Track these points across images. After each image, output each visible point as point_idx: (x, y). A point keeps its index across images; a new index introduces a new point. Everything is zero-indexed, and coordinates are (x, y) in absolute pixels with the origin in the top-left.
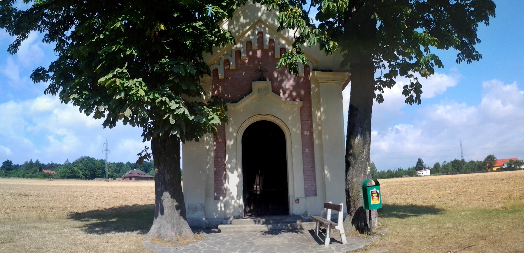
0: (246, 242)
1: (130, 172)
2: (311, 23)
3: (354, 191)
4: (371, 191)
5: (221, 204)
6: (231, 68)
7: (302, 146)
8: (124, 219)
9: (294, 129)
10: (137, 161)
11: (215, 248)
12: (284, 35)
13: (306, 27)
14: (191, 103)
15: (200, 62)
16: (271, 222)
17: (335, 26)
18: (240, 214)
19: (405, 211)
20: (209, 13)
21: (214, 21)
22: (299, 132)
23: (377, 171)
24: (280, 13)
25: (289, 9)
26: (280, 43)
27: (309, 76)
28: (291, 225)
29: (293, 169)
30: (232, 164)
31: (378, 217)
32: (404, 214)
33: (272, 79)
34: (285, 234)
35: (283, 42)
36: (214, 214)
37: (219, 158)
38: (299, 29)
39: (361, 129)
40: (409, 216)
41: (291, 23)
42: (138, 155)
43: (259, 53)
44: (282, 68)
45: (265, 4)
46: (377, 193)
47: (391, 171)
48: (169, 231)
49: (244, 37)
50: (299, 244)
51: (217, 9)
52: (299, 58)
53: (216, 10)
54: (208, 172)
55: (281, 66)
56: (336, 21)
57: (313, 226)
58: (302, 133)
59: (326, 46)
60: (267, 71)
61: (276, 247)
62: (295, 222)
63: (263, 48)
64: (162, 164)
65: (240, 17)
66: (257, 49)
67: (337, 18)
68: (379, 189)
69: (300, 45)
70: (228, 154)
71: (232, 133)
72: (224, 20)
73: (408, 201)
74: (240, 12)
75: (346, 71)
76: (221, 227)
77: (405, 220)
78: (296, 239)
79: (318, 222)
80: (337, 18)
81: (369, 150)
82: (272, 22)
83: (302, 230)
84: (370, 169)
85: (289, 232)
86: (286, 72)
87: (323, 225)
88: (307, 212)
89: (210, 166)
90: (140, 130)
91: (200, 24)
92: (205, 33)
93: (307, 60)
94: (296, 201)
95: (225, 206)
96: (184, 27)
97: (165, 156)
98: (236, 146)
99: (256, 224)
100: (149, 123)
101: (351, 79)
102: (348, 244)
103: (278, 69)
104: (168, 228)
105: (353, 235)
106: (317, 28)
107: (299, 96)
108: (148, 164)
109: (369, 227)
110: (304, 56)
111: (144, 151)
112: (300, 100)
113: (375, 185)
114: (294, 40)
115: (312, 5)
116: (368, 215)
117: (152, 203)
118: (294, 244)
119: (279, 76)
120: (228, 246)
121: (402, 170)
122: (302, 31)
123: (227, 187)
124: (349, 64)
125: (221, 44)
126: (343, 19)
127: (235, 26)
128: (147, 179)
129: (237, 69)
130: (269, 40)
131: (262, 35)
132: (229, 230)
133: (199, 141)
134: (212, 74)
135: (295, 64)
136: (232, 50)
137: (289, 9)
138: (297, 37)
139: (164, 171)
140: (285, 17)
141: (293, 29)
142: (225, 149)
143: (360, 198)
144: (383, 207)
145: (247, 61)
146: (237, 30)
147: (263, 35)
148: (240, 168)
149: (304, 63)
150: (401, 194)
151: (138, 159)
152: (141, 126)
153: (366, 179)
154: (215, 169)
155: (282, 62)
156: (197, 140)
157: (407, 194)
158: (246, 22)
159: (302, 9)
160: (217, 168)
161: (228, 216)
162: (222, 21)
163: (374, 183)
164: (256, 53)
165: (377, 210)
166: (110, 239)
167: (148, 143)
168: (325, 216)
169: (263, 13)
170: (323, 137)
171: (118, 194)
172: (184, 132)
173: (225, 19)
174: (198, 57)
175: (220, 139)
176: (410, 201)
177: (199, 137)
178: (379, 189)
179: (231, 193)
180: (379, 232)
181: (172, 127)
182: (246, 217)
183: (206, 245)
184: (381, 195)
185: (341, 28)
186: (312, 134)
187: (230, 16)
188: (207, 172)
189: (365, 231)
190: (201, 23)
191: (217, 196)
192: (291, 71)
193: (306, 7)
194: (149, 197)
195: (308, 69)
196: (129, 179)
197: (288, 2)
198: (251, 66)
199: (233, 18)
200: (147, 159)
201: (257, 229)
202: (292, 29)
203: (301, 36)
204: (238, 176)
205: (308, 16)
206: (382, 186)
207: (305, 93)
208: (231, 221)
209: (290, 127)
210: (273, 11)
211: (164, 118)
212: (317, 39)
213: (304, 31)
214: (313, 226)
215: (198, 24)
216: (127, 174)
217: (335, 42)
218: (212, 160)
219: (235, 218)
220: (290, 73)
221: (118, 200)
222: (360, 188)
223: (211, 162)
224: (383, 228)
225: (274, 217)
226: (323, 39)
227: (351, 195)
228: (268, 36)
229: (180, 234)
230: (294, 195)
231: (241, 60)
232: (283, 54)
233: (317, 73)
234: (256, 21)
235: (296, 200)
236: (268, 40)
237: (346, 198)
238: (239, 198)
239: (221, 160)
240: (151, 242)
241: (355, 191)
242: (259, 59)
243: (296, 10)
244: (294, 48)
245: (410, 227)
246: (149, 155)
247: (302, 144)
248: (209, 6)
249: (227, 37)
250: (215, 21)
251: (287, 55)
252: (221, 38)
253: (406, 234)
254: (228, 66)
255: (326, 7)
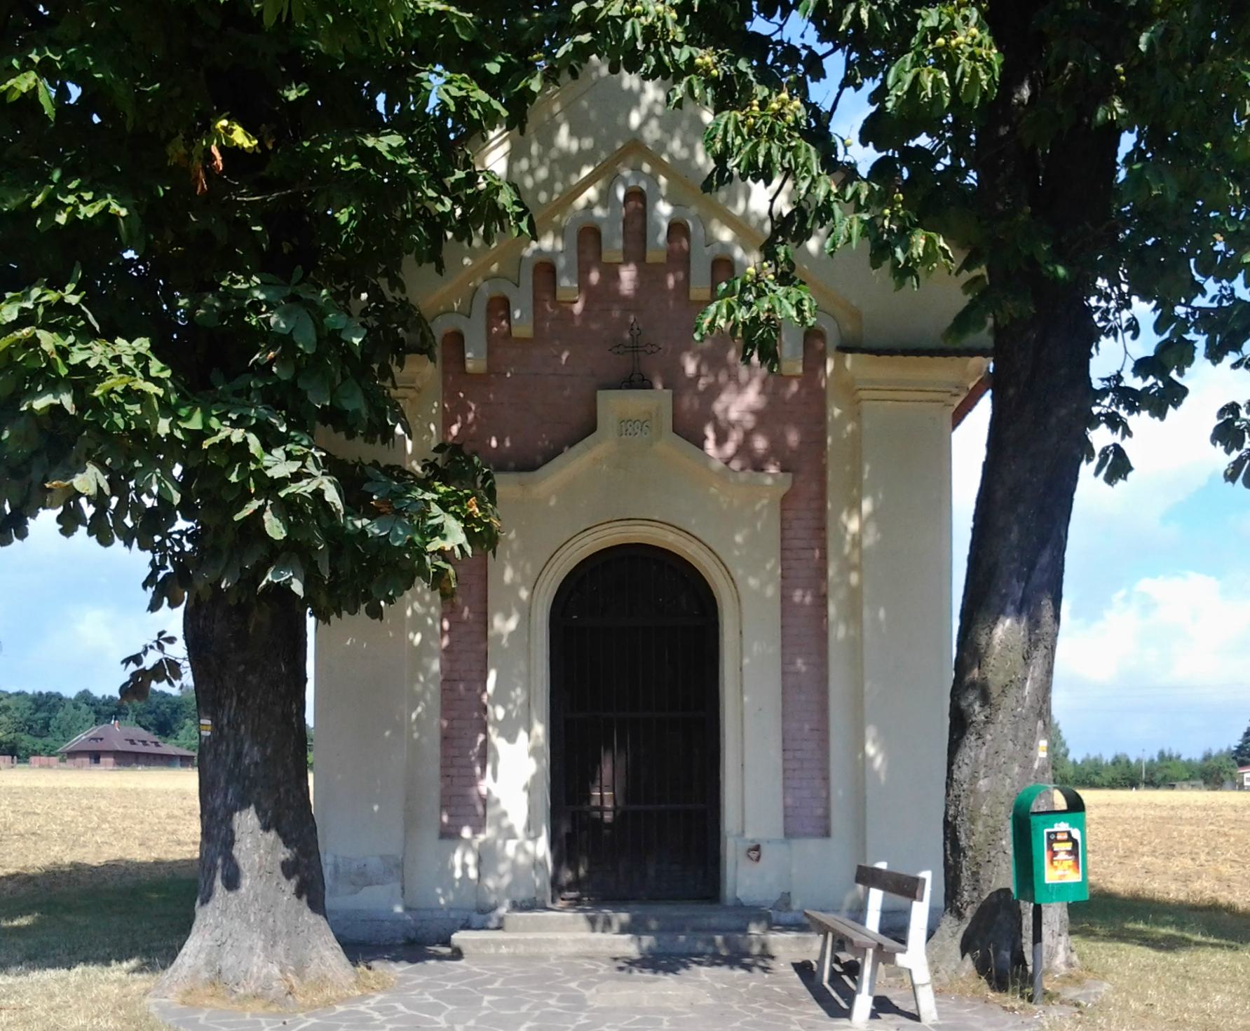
0: (558, 994)
1: (94, 731)
2: (839, 159)
3: (980, 827)
4: (1046, 831)
5: (463, 856)
6: (517, 332)
7: (783, 646)
8: (70, 918)
9: (753, 582)
10: (124, 689)
11: (436, 1019)
12: (729, 208)
13: (819, 175)
14: (356, 464)
15: (390, 300)
16: (653, 925)
17: (940, 167)
18: (537, 891)
19: (1181, 925)
20: (433, 101)
21: (452, 136)
22: (772, 591)
23: (1071, 757)
24: (715, 114)
25: (755, 102)
26: (712, 238)
27: (821, 372)
28: (727, 942)
29: (742, 734)
30: (510, 707)
31: (1071, 933)
32: (1178, 934)
33: (675, 380)
34: (704, 973)
35: (726, 235)
36: (439, 891)
37: (462, 680)
38: (789, 184)
39: (1023, 584)
40: (1198, 944)
41: (761, 160)
42: (127, 661)
43: (627, 276)
44: (714, 340)
45: (659, 79)
46: (1070, 839)
47: (1128, 762)
48: (255, 959)
49: (570, 211)
50: (753, 1010)
51: (464, 85)
52: (785, 301)
53: (460, 89)
54: (416, 735)
55: (712, 332)
56: (945, 145)
57: (812, 947)
58: (785, 598)
59: (898, 250)
60: (655, 349)
61: (666, 1018)
62: (744, 930)
63: (644, 259)
64: (227, 702)
65: (558, 127)
66: (621, 260)
67: (948, 135)
68: (1082, 826)
69: (791, 246)
70: (495, 667)
71: (513, 588)
72: (492, 135)
73: (1197, 885)
74: (557, 108)
75: (971, 352)
76: (465, 940)
77: (1182, 960)
78: (742, 990)
79: (830, 935)
80: (948, 135)
81: (1049, 672)
82: (683, 154)
83: (769, 961)
84: (1049, 749)
85: (719, 965)
86: (732, 354)
87: (847, 946)
88: (789, 894)
89: (426, 710)
90: (138, 561)
91: (395, 145)
92: (413, 184)
93: (817, 310)
94: (751, 854)
95: (479, 862)
96: (328, 147)
97: (242, 668)
98: (526, 639)
99: (594, 930)
100: (177, 536)
101: (996, 383)
102: (940, 1023)
103: (700, 344)
104: (251, 948)
105: (962, 992)
106: (865, 176)
107: (776, 450)
108: (168, 703)
109: (1030, 969)
110: (806, 292)
111: (152, 647)
112: (783, 470)
113: (1064, 807)
114: (768, 227)
115: (848, 81)
116: (1027, 921)
117: (189, 856)
118: (736, 1007)
119: (704, 370)
120: (487, 1008)
121: (1179, 757)
122: (803, 192)
123: (489, 791)
124: (990, 322)
125: (478, 235)
126: (973, 137)
127: (535, 162)
128: (166, 760)
129: (539, 336)
130: (670, 227)
131: (640, 205)
132: (492, 950)
133: (381, 619)
134: (438, 352)
135: (768, 325)
136: (521, 258)
137: (755, 102)
138: (781, 214)
139: (238, 729)
140: (738, 132)
141: (768, 183)
142: (483, 646)
143: (1001, 855)
144: (1092, 896)
145: (578, 308)
146: (545, 181)
147: (644, 204)
148: (541, 722)
149: (803, 320)
150: (1169, 856)
151: (128, 679)
152: (142, 547)
153: (1032, 784)
154: (445, 724)
155: (716, 316)
156: (376, 613)
157: (1193, 859)
158: (580, 148)
159: (804, 101)
160: (451, 720)
161: (492, 899)
162: (484, 139)
163: (1060, 802)
164: (617, 277)
165: (1069, 906)
166: (9, 997)
167: (172, 619)
168: (859, 913)
169: (650, 115)
170: (866, 614)
171: (41, 821)
172: (323, 578)
173: (497, 131)
174: (386, 280)
175: (466, 609)
176: (1205, 889)
177: (382, 603)
178: (1082, 826)
179: (504, 814)
180: (1072, 993)
181: (275, 553)
182: (560, 904)
183: (401, 1007)
184: (1089, 848)
185: (964, 172)
186: (822, 601)
187: (517, 121)
188: (412, 732)
189: (1014, 983)
190: (396, 140)
191: (449, 825)
192: (752, 354)
193: (820, 93)
194: (174, 832)
195: (820, 345)
196: (88, 759)
197: (749, 71)
198: (594, 326)
199: (529, 128)
200: (165, 682)
201: (600, 949)
202: (761, 182)
203: (799, 209)
204: (534, 752)
205: (828, 127)
206: (1094, 816)
207: (801, 443)
208: (501, 919)
209: (738, 573)
210: (689, 106)
211: (237, 517)
212: (862, 221)
213: (808, 190)
214: (812, 947)
215: (386, 143)
216: (80, 739)
217: (933, 234)
218: (434, 688)
219: (517, 906)
220: (746, 359)
221: (42, 845)
222: (1002, 817)
223: (428, 696)
224: (1087, 981)
225: (664, 909)
226: (886, 223)
227: (963, 843)
228: (664, 209)
229: (300, 971)
230: (743, 832)
231: (555, 303)
232: (724, 286)
233: (853, 361)
234: (619, 145)
235: (750, 850)
236: (665, 225)
237: (945, 850)
238: (532, 834)
239: (468, 690)
240: (184, 1003)
241: (980, 828)
242: (625, 299)
243: (783, 105)
244: (766, 260)
245: (1205, 989)
246: (174, 666)
247: (782, 640)
248: (432, 72)
249: (501, 207)
250: (456, 137)
251: (738, 287)
252: (479, 210)
253: (1186, 1015)
254: (504, 323)
255: (906, 87)
